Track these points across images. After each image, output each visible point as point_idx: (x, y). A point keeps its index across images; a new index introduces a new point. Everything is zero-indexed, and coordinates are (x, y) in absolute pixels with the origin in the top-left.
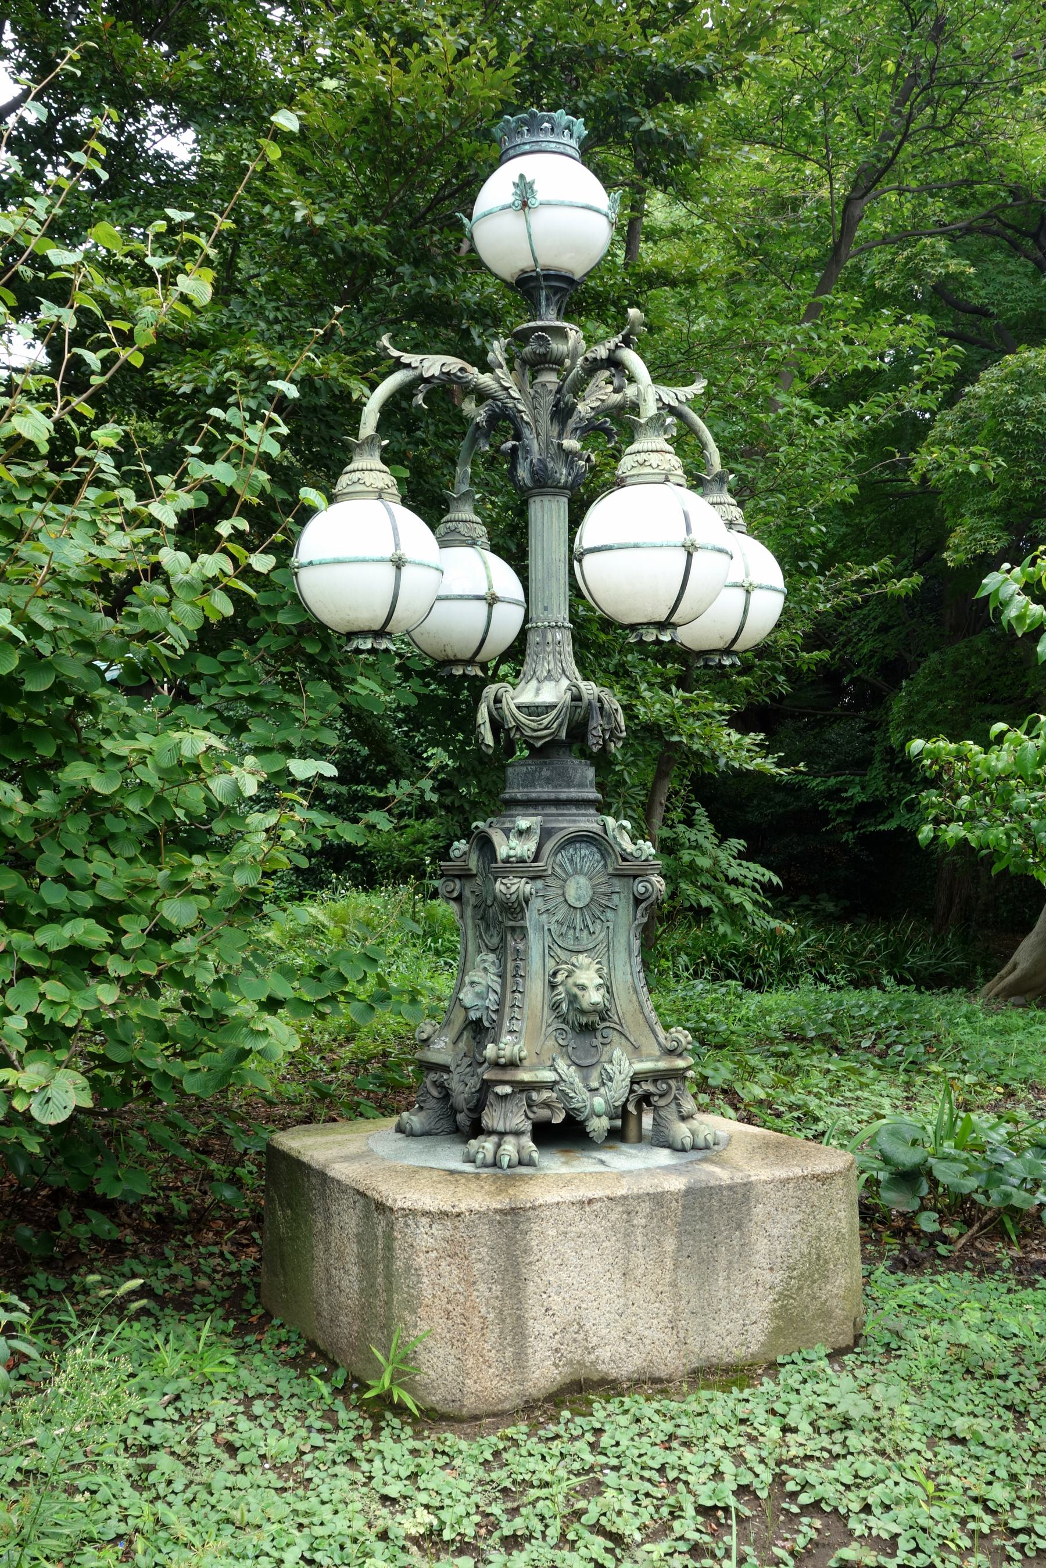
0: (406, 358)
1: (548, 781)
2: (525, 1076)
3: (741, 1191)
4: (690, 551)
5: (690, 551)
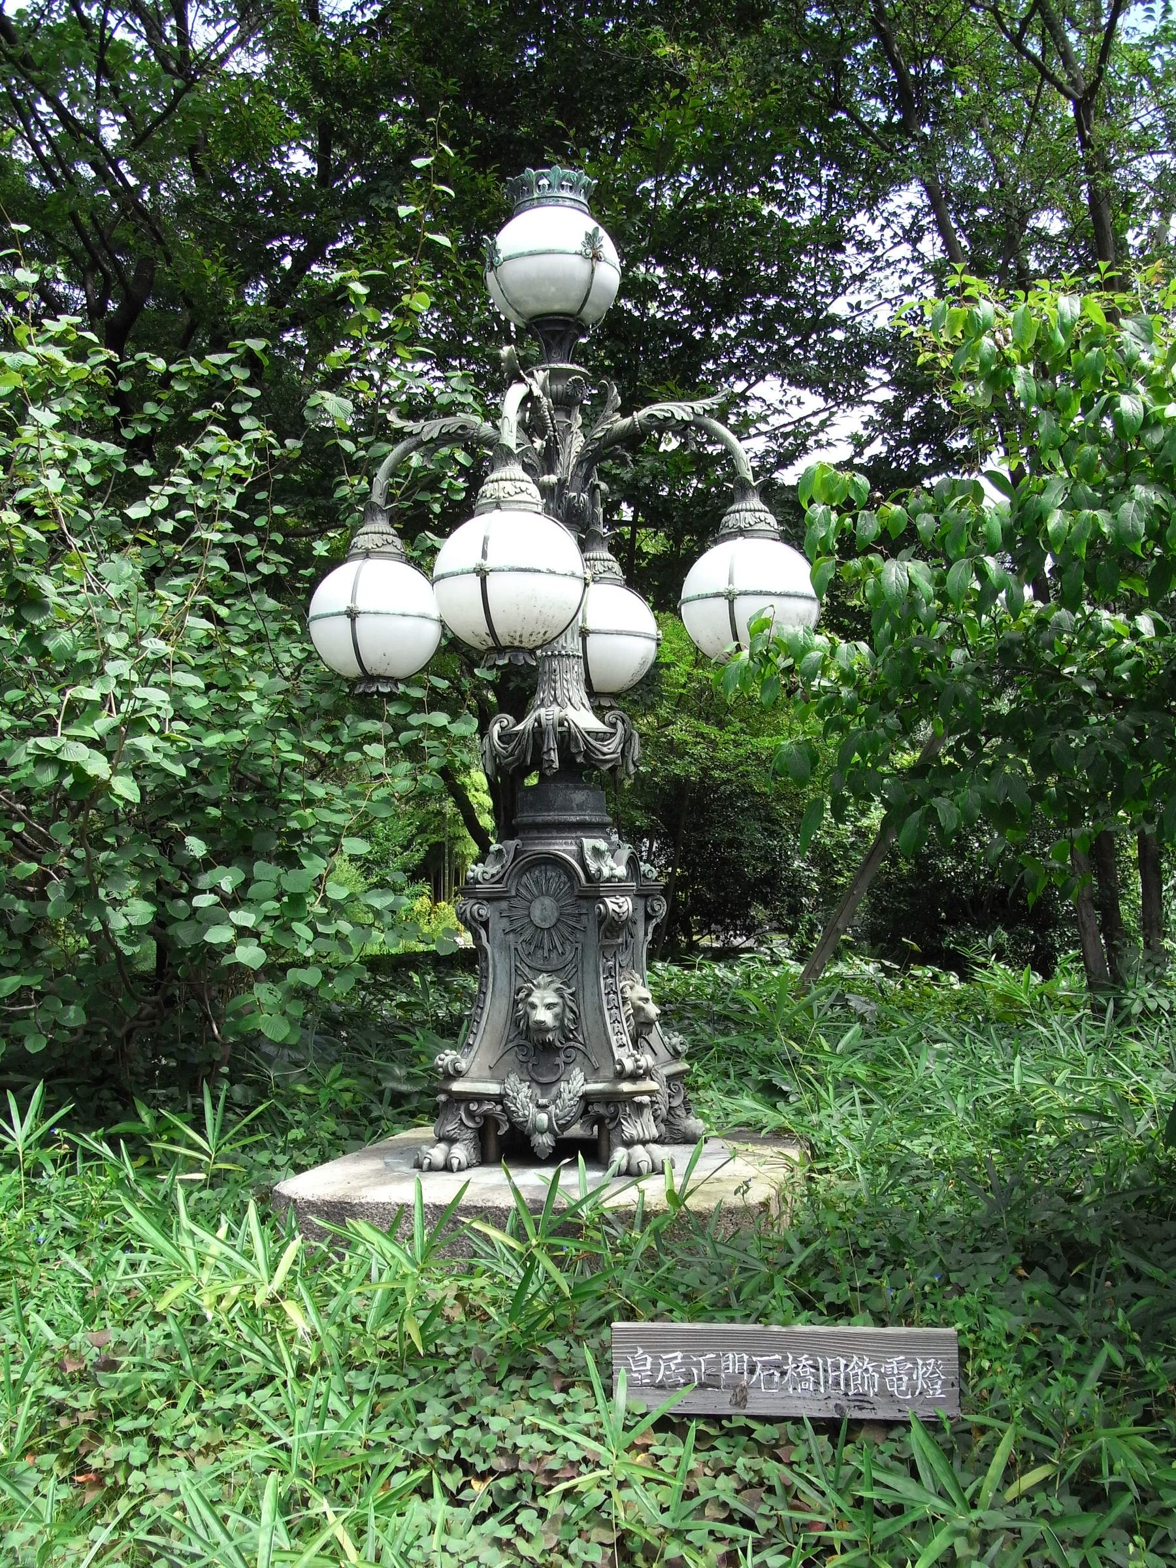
2: (457, 1086)
4: (482, 574)
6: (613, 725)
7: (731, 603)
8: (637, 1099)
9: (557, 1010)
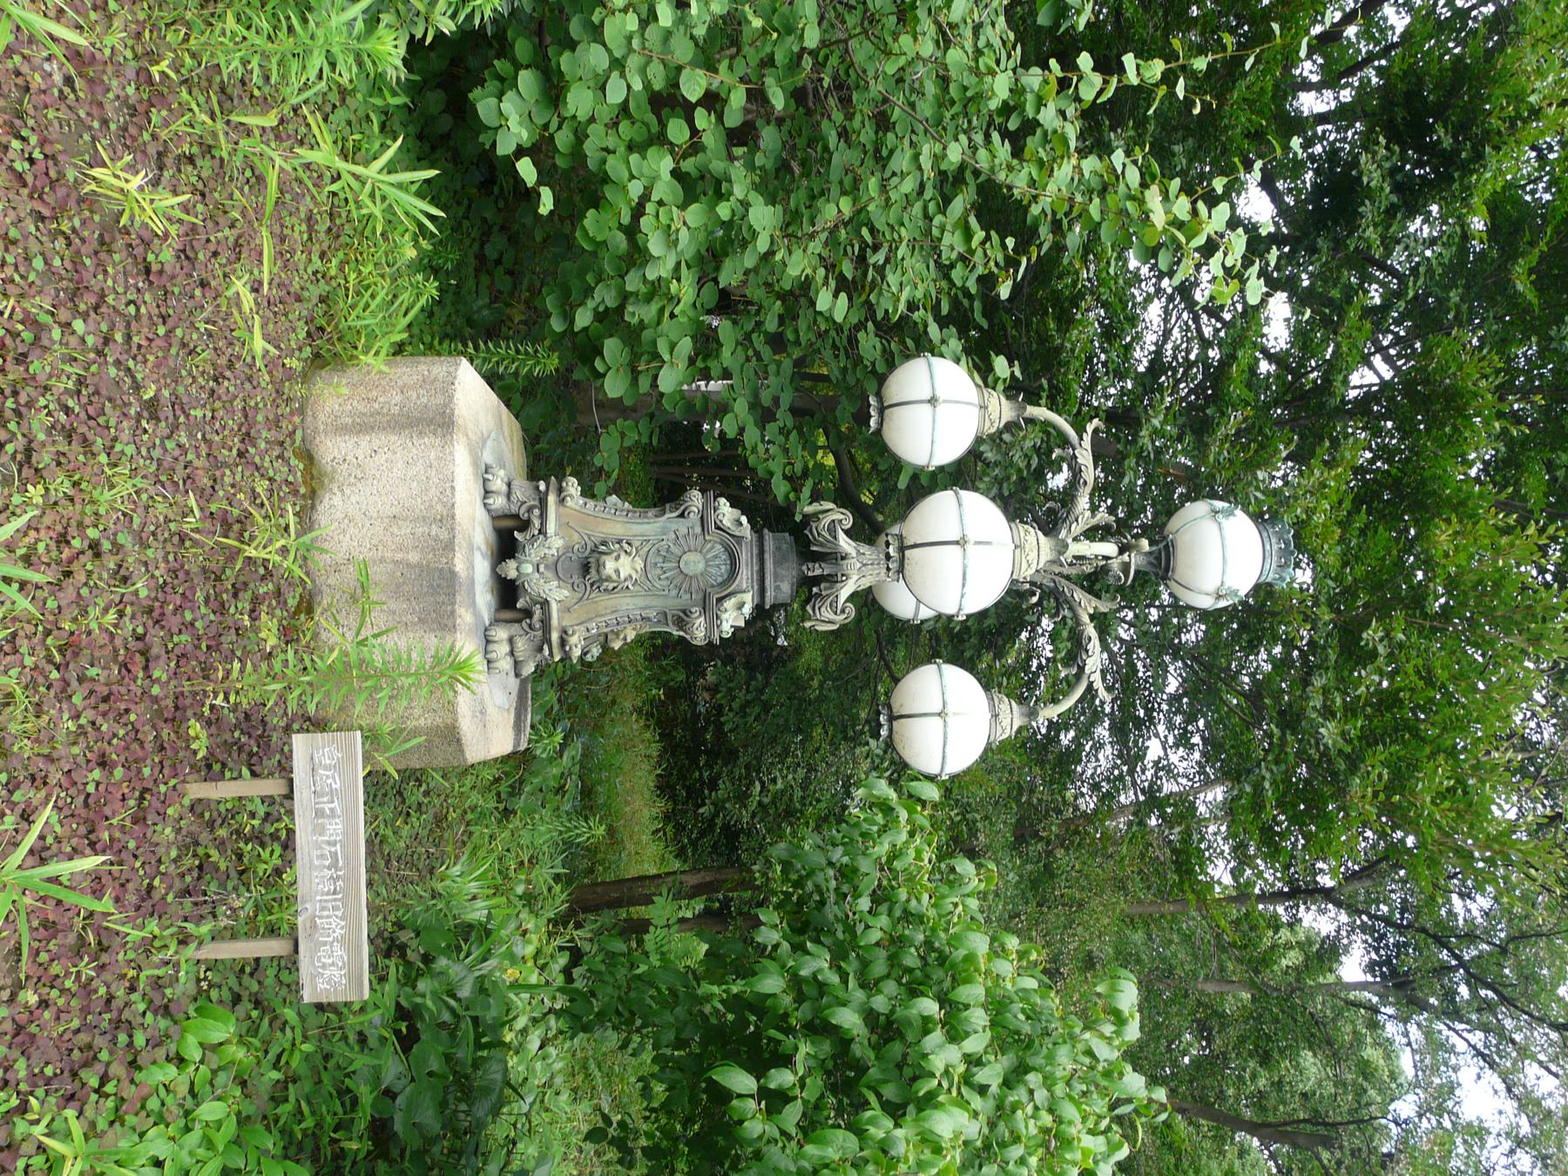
0: (1087, 438)
1: (778, 549)
2: (552, 498)
3: (450, 623)
4: (960, 543)
5: (960, 543)
6: (843, 611)
7: (957, 543)
8: (546, 647)
9: (614, 577)
